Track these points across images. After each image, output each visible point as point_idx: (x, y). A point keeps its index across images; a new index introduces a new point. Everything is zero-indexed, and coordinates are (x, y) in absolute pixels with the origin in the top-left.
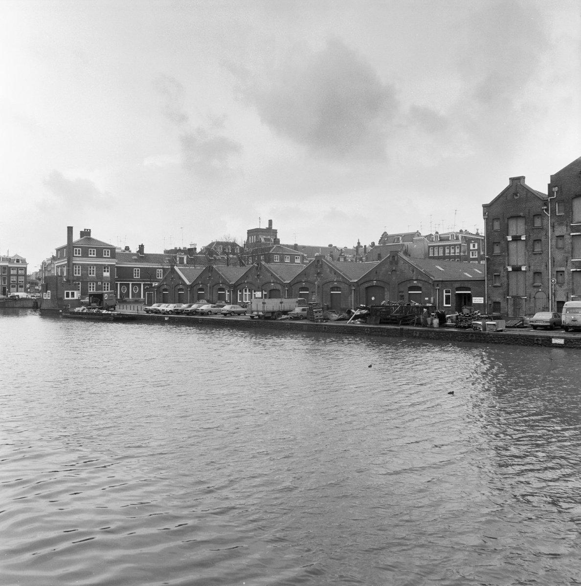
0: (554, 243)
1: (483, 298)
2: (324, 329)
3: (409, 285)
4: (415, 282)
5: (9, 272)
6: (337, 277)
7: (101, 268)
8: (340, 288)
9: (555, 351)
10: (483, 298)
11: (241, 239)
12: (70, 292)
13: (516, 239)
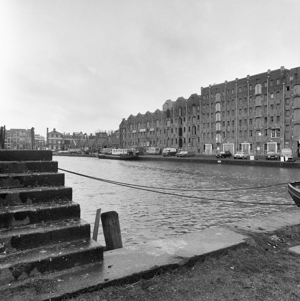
0: (175, 121)
5: (38, 142)
7: (57, 140)
9: (218, 165)
12: (45, 148)
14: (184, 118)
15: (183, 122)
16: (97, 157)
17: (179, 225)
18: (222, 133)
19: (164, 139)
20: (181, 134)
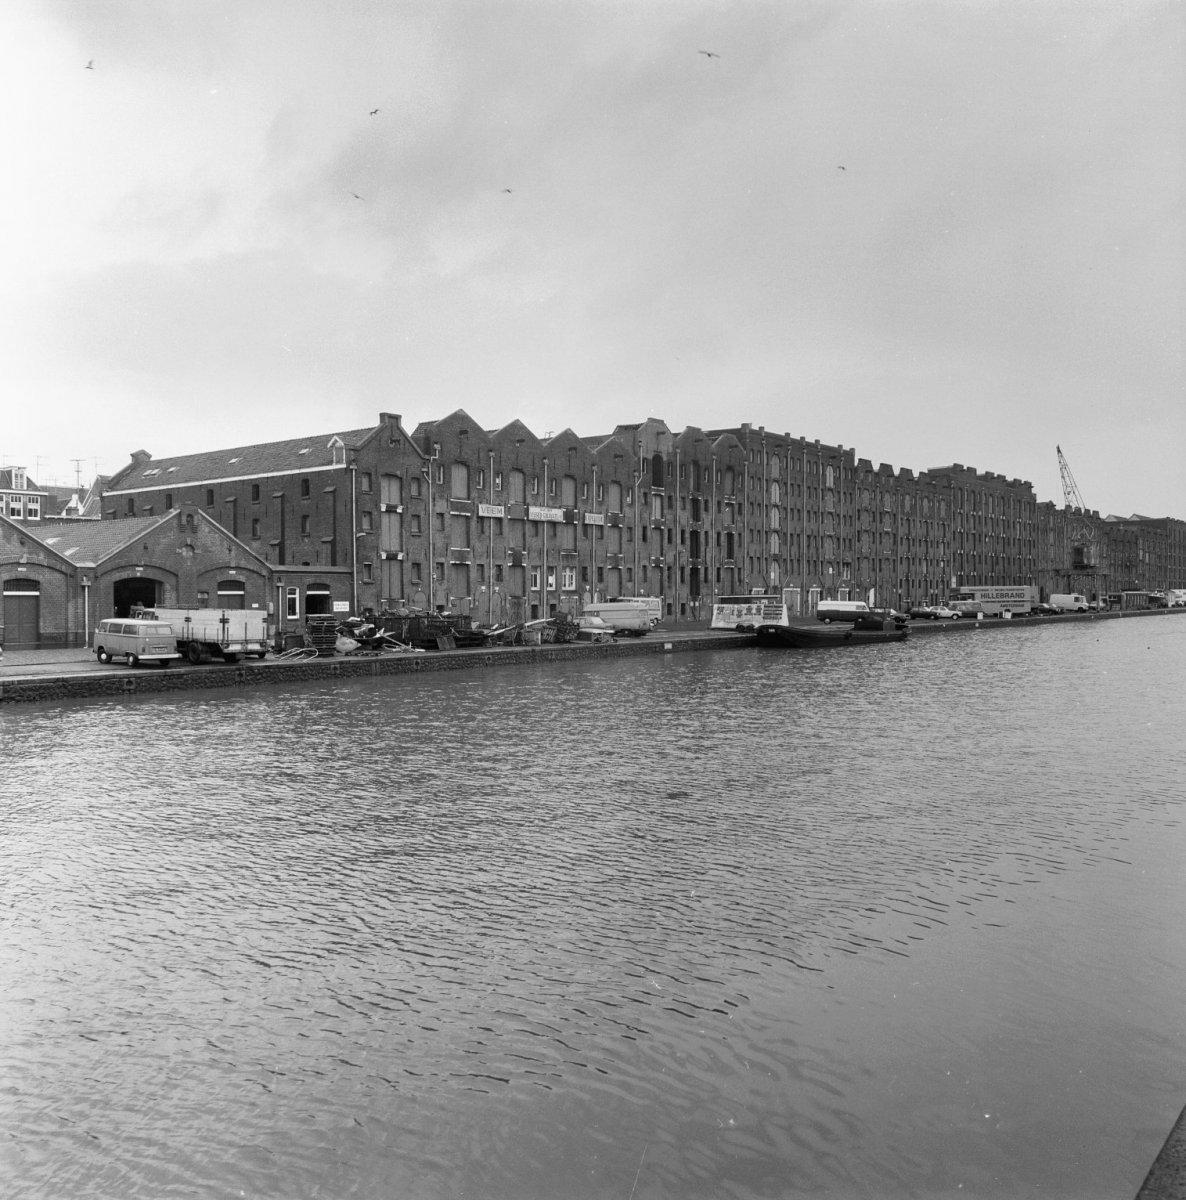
1: (348, 603)
2: (415, 667)
3: (220, 579)
4: (233, 572)
6: (30, 553)
8: (38, 582)
10: (348, 603)
11: (1060, 506)
13: (391, 510)
14: (706, 502)
15: (703, 515)
16: (978, 628)
17: (482, 902)
18: (781, 561)
19: (642, 564)
20: (695, 552)
